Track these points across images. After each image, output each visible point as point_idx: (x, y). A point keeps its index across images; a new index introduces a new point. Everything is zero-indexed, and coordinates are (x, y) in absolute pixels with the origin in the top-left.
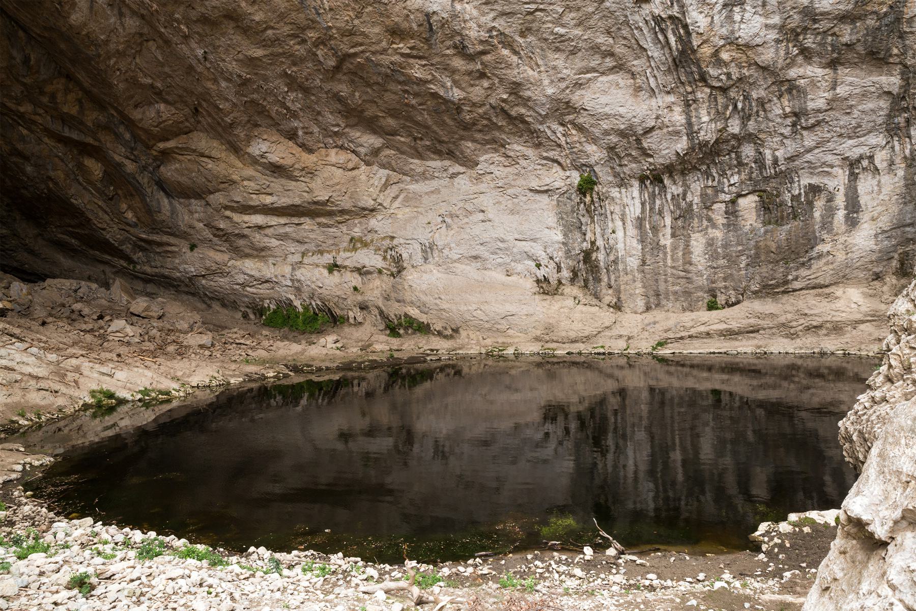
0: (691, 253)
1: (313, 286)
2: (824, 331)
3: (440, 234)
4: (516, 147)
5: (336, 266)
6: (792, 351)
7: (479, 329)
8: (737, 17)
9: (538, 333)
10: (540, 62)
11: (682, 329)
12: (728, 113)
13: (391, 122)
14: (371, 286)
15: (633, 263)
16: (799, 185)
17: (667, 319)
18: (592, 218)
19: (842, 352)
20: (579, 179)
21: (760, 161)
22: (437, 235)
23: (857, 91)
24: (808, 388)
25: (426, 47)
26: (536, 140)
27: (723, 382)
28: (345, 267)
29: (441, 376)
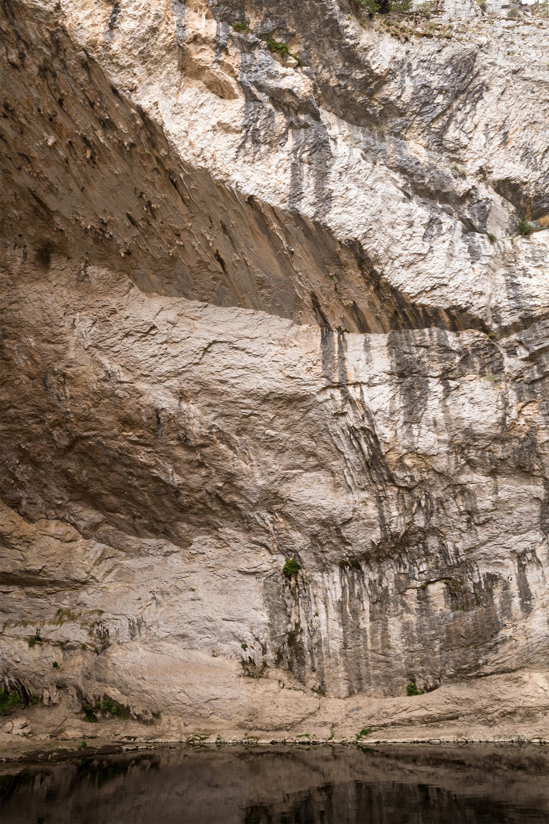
0: (389, 636)
1: (10, 660)
2: (518, 718)
3: (150, 611)
4: (227, 530)
5: (38, 638)
6: (491, 739)
7: (181, 714)
8: (415, 432)
9: (242, 719)
10: (253, 457)
11: (385, 715)
12: (414, 509)
13: (113, 500)
14: (72, 662)
15: (336, 645)
16: (479, 574)
17: (370, 704)
18: (297, 600)
19: (537, 741)
20: (284, 563)
21: (443, 551)
22: (146, 612)
23: (513, 496)
24: (513, 781)
25: (153, 437)
26: (247, 526)
27: (429, 775)
28: (48, 641)
29: (135, 771)
